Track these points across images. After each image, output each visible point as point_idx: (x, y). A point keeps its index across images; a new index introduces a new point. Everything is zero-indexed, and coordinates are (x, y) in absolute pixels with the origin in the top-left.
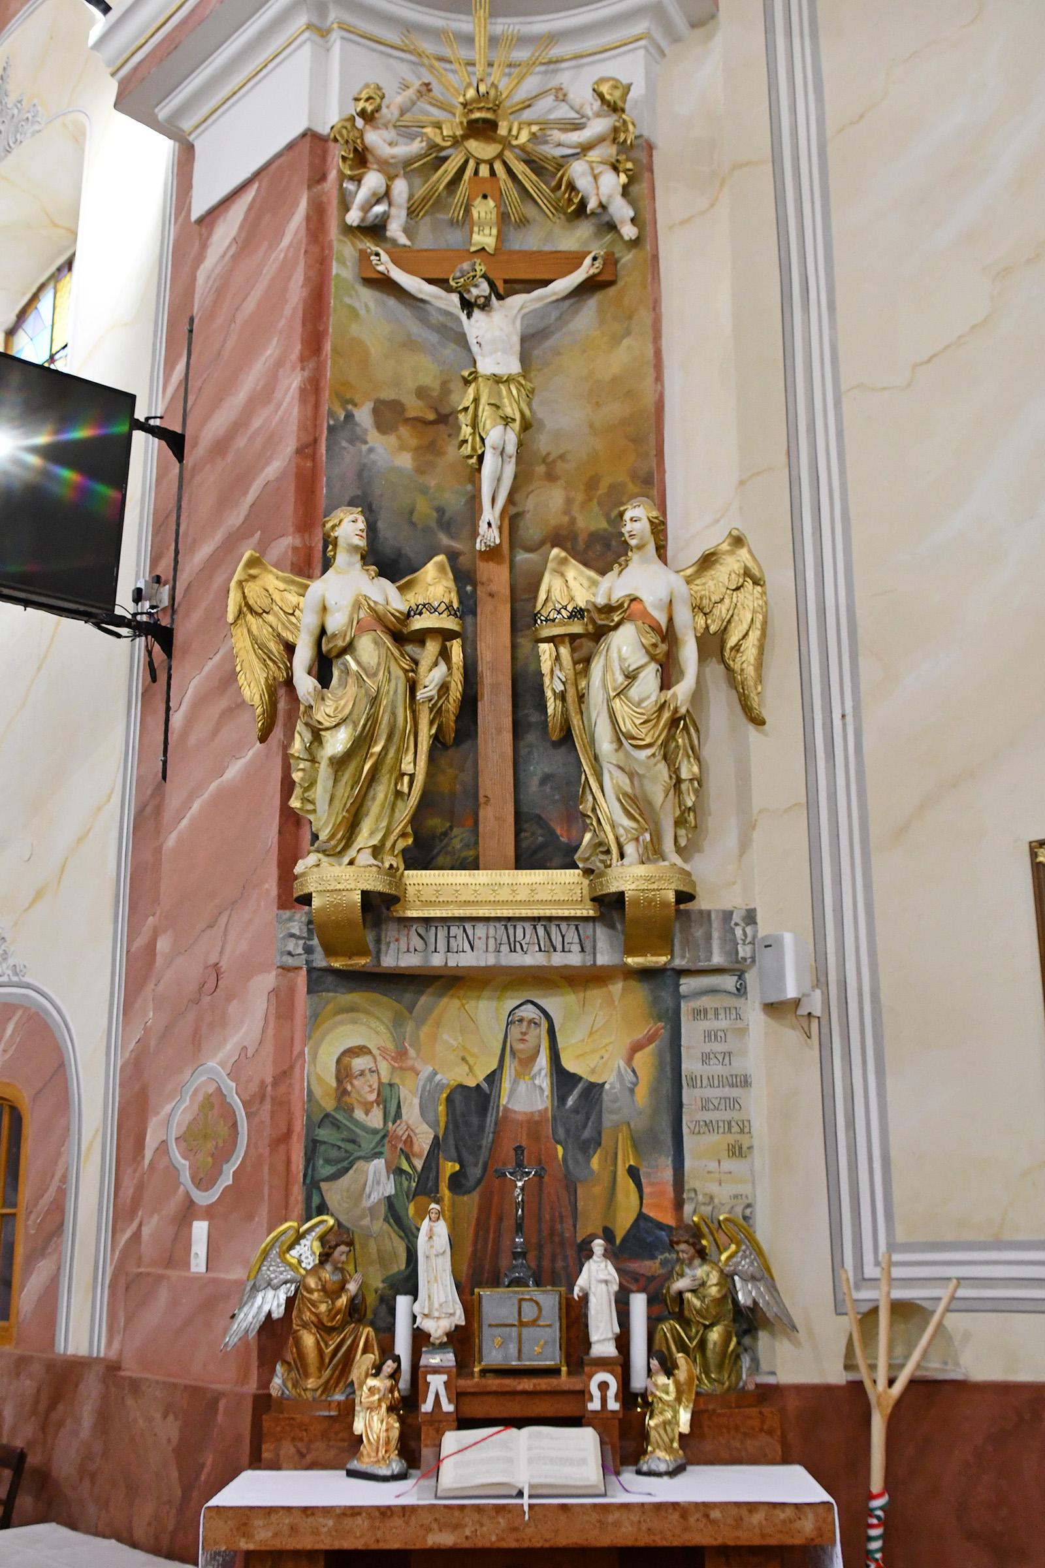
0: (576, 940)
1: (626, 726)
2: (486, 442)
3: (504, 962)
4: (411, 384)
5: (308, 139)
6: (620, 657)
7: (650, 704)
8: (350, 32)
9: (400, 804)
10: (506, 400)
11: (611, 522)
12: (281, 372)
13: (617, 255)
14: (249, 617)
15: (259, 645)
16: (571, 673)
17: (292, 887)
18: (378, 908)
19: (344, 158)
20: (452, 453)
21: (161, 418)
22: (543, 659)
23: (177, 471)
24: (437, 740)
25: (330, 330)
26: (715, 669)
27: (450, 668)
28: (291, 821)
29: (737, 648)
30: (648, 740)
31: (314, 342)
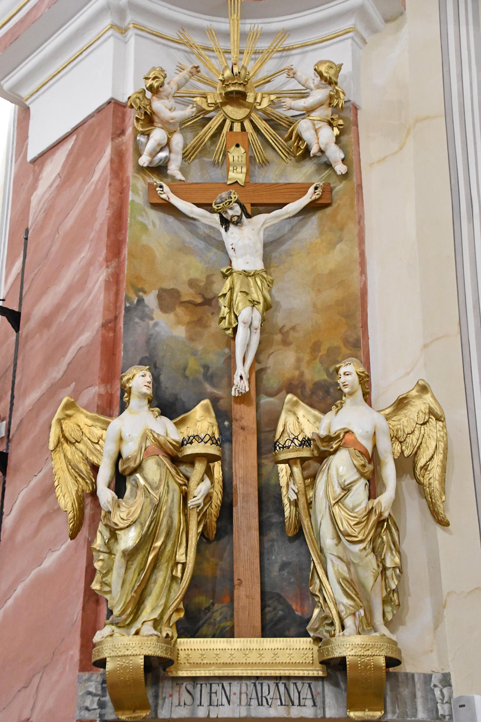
0: (309, 696)
1: (344, 526)
2: (239, 318)
3: (254, 714)
4: (184, 277)
5: (112, 105)
6: (338, 474)
7: (361, 509)
8: (142, 30)
9: (175, 586)
10: (253, 289)
11: (330, 375)
12: (91, 268)
13: (332, 185)
14: (65, 445)
15: (71, 465)
16: (302, 486)
17: (91, 654)
18: (157, 669)
19: (137, 119)
20: (214, 326)
21: (3, 300)
22: (281, 475)
23: (14, 338)
24: (203, 536)
25: (127, 240)
26: (409, 483)
27: (212, 483)
28: (93, 600)
29: (425, 467)
30: (360, 537)
31: (115, 248)
